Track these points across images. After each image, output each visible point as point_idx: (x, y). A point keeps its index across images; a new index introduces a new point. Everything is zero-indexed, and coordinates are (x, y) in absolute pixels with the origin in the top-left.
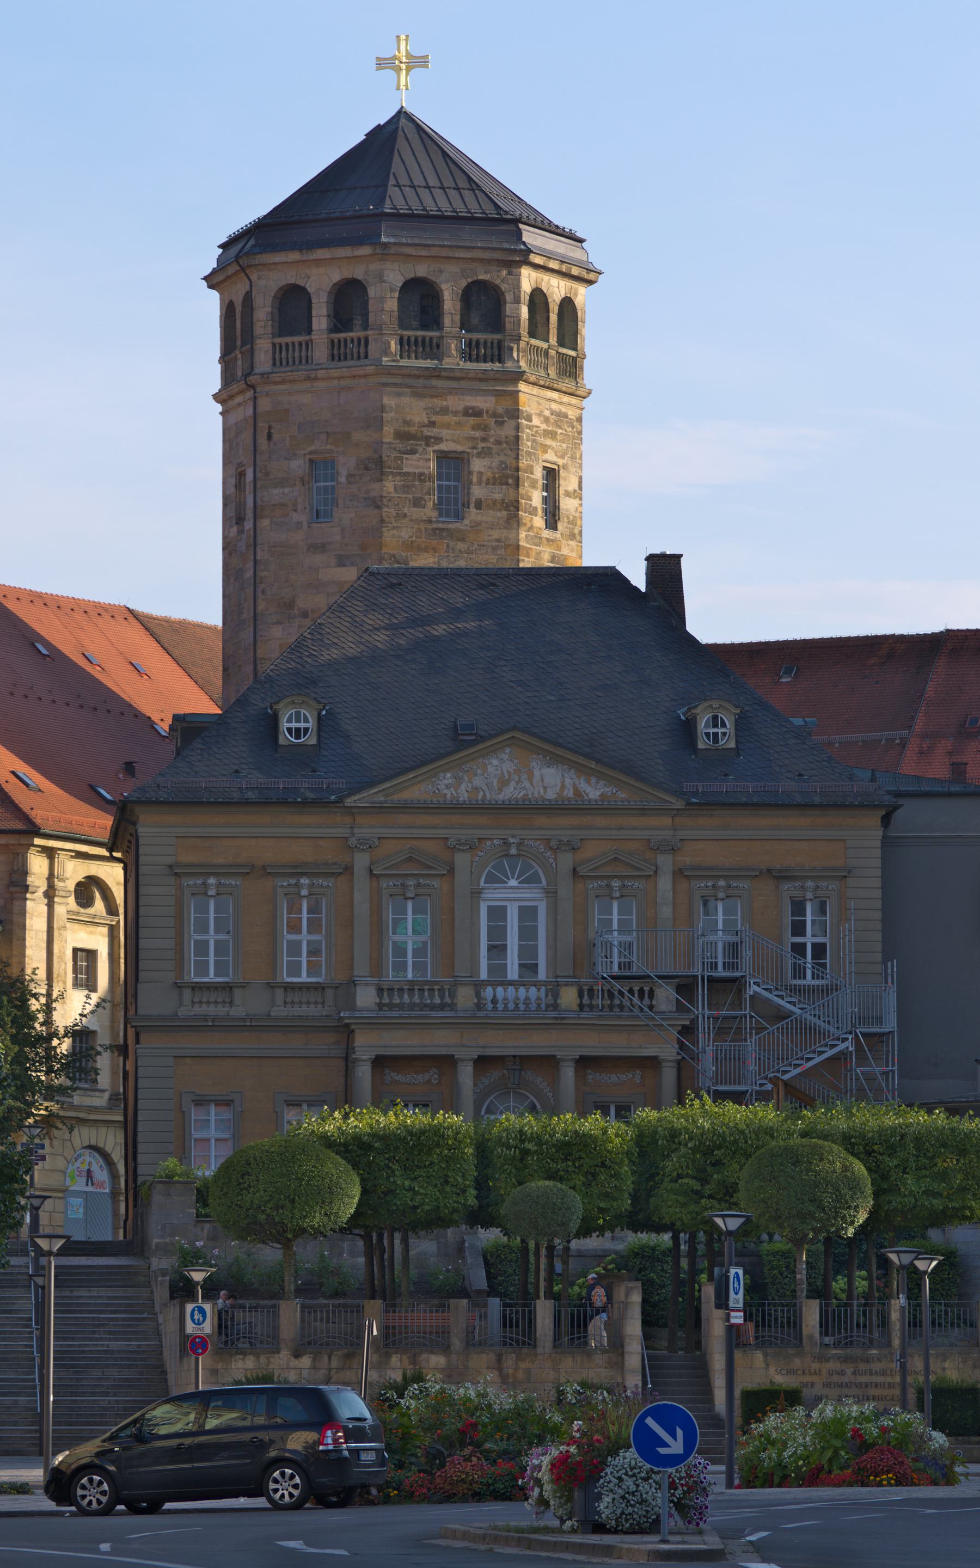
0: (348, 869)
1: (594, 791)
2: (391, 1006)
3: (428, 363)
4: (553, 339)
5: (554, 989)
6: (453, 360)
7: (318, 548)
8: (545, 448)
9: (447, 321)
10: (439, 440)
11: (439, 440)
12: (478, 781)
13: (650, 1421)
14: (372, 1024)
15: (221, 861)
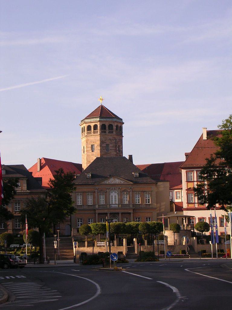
0: (95, 192)
1: (122, 182)
2: (100, 207)
3: (105, 134)
4: (119, 131)
5: (118, 205)
6: (92, 133)
7: (92, 155)
8: (118, 143)
9: (107, 129)
10: (106, 142)
11: (106, 142)
12: (109, 181)
13: (112, 255)
14: (98, 209)
15: (80, 191)
